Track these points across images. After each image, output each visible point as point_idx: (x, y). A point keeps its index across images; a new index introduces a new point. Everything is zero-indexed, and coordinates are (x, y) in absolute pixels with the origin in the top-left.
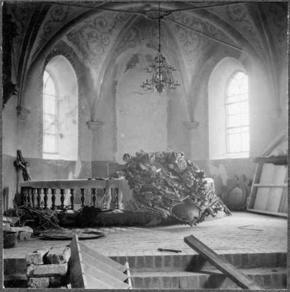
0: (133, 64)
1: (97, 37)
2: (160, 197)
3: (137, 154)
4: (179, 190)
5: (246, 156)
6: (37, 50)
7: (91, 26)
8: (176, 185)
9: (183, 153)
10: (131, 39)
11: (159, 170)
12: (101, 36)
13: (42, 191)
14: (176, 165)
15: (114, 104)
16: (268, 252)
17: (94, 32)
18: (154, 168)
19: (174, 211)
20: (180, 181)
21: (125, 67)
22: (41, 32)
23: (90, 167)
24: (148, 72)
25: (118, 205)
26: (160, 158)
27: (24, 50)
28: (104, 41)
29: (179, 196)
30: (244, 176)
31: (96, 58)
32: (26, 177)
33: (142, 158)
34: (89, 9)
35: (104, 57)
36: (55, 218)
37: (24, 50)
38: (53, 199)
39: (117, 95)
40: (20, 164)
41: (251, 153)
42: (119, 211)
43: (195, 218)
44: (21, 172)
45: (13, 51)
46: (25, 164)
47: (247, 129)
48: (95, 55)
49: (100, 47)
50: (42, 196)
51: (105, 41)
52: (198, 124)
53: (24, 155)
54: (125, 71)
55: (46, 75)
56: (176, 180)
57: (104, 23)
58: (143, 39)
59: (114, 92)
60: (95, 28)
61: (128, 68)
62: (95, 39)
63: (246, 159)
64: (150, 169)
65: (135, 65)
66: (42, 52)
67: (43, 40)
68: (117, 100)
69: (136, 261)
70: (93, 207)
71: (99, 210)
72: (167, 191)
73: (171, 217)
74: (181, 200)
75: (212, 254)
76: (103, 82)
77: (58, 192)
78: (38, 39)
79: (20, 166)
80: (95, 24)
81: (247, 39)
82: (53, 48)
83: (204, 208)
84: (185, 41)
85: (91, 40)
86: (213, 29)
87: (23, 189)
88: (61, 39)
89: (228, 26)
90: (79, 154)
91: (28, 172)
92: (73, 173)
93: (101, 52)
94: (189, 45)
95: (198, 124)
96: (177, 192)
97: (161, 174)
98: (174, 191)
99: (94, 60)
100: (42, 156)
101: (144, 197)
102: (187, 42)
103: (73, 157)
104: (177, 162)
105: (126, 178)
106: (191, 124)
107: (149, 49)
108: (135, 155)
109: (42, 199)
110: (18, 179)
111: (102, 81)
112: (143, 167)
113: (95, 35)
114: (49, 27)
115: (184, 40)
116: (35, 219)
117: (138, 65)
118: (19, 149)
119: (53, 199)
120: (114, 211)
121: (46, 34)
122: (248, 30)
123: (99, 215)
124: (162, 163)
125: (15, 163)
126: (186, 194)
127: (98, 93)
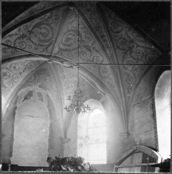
0: (29, 97)
1: (9, 76)
5: (105, 162)
7: (7, 68)
10: (30, 80)
12: (13, 75)
15: (13, 122)
17: (9, 72)
21: (23, 98)
28: (14, 79)
31: (6, 89)
34: (29, 53)
35: (12, 90)
39: (16, 116)
41: (108, 161)
45: (142, 41)
48: (6, 87)
49: (11, 83)
51: (16, 80)
54: (23, 101)
57: (17, 68)
58: (38, 82)
59: (14, 114)
60: (10, 70)
61: (25, 99)
62: (8, 77)
63: (105, 164)
65: (30, 98)
68: (15, 120)
76: (9, 107)
80: (10, 67)
81: (110, 89)
84: (67, 86)
85: (5, 77)
86: (83, 81)
89: (99, 80)
93: (11, 86)
94: (69, 89)
95: (69, 140)
99: (4, 91)
102: (68, 87)
104: (82, 165)
106: (65, 139)
107: (40, 88)
111: (8, 105)
113: (8, 74)
115: (66, 86)
117: (32, 98)
122: (110, 84)
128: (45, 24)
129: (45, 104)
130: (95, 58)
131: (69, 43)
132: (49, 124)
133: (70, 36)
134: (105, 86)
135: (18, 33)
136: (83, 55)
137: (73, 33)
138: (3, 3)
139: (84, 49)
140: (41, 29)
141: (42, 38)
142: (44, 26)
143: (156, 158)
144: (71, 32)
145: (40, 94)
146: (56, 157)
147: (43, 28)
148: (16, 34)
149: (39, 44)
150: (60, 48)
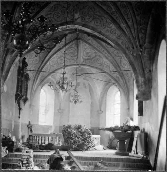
2: (73, 141)
3: (68, 125)
4: (81, 139)
6: (38, 84)
8: (80, 137)
9: (85, 125)
11: (75, 131)
13: (35, 137)
14: (81, 130)
16: (89, 156)
18: (73, 130)
19: (78, 146)
20: (82, 136)
22: (40, 76)
23: (58, 128)
24: (58, 110)
25: (60, 143)
26: (76, 127)
27: (33, 83)
29: (80, 141)
30: (144, 129)
32: (31, 131)
33: (70, 127)
36: (38, 146)
37: (33, 83)
38: (42, 140)
40: (29, 127)
42: (60, 145)
43: (85, 149)
44: (30, 129)
46: (31, 126)
47: (119, 115)
50: (38, 139)
52: (102, 112)
53: (31, 123)
55: (42, 91)
56: (80, 135)
64: (71, 131)
66: (41, 83)
67: (41, 80)
69: (46, 156)
70: (51, 144)
71: (53, 145)
72: (76, 139)
73: (76, 148)
74: (81, 142)
75: (72, 156)
77: (43, 138)
78: (39, 79)
79: (30, 127)
82: (45, 81)
83: (89, 146)
87: (30, 136)
88: (49, 77)
90: (54, 123)
91: (32, 130)
92: (51, 130)
95: (102, 112)
96: (80, 139)
97: (75, 133)
98: (79, 139)
100: (38, 123)
101: (67, 140)
103: (52, 124)
105: (63, 134)
107: (84, 80)
108: (67, 126)
109: (35, 140)
110: (29, 132)
112: (69, 130)
114: (17, 161)
116: (31, 146)
117: (79, 87)
118: (30, 121)
119: (42, 140)
120: (58, 145)
121: (42, 77)
123: (53, 146)
124: (77, 129)
125: (28, 126)
126: (83, 140)
127: (63, 98)
128: (71, 48)
129: (88, 90)
130: (106, 62)
131: (89, 55)
132: (90, 102)
133: (88, 51)
134: (107, 85)
135: (57, 56)
136: (98, 61)
137: (90, 49)
138: (164, 3)
139: (98, 57)
140: (70, 50)
141: (72, 55)
142: (71, 49)
143: (116, 159)
144: (89, 49)
145: (84, 84)
146: (78, 125)
147: (72, 50)
148: (56, 57)
149: (71, 59)
150: (84, 59)
